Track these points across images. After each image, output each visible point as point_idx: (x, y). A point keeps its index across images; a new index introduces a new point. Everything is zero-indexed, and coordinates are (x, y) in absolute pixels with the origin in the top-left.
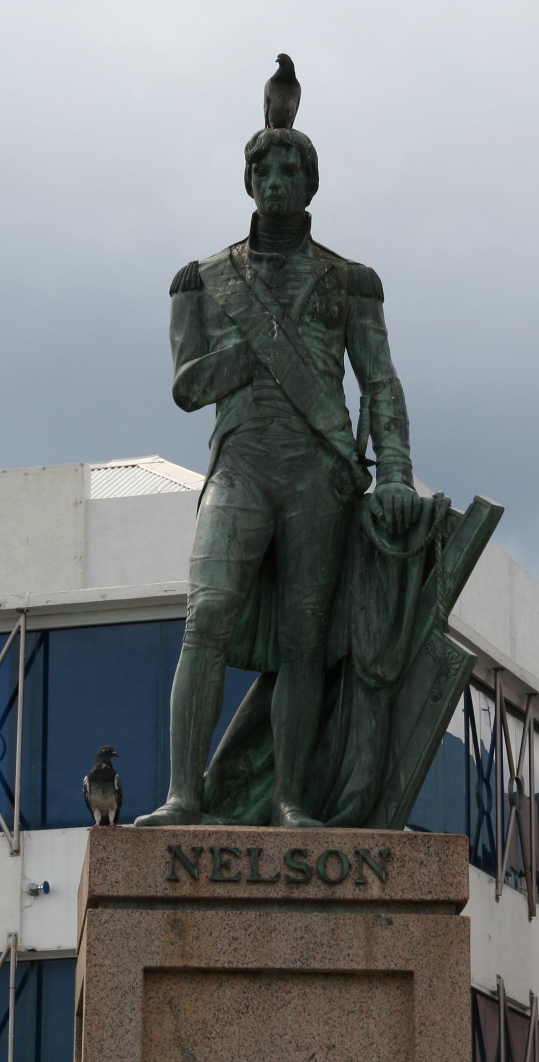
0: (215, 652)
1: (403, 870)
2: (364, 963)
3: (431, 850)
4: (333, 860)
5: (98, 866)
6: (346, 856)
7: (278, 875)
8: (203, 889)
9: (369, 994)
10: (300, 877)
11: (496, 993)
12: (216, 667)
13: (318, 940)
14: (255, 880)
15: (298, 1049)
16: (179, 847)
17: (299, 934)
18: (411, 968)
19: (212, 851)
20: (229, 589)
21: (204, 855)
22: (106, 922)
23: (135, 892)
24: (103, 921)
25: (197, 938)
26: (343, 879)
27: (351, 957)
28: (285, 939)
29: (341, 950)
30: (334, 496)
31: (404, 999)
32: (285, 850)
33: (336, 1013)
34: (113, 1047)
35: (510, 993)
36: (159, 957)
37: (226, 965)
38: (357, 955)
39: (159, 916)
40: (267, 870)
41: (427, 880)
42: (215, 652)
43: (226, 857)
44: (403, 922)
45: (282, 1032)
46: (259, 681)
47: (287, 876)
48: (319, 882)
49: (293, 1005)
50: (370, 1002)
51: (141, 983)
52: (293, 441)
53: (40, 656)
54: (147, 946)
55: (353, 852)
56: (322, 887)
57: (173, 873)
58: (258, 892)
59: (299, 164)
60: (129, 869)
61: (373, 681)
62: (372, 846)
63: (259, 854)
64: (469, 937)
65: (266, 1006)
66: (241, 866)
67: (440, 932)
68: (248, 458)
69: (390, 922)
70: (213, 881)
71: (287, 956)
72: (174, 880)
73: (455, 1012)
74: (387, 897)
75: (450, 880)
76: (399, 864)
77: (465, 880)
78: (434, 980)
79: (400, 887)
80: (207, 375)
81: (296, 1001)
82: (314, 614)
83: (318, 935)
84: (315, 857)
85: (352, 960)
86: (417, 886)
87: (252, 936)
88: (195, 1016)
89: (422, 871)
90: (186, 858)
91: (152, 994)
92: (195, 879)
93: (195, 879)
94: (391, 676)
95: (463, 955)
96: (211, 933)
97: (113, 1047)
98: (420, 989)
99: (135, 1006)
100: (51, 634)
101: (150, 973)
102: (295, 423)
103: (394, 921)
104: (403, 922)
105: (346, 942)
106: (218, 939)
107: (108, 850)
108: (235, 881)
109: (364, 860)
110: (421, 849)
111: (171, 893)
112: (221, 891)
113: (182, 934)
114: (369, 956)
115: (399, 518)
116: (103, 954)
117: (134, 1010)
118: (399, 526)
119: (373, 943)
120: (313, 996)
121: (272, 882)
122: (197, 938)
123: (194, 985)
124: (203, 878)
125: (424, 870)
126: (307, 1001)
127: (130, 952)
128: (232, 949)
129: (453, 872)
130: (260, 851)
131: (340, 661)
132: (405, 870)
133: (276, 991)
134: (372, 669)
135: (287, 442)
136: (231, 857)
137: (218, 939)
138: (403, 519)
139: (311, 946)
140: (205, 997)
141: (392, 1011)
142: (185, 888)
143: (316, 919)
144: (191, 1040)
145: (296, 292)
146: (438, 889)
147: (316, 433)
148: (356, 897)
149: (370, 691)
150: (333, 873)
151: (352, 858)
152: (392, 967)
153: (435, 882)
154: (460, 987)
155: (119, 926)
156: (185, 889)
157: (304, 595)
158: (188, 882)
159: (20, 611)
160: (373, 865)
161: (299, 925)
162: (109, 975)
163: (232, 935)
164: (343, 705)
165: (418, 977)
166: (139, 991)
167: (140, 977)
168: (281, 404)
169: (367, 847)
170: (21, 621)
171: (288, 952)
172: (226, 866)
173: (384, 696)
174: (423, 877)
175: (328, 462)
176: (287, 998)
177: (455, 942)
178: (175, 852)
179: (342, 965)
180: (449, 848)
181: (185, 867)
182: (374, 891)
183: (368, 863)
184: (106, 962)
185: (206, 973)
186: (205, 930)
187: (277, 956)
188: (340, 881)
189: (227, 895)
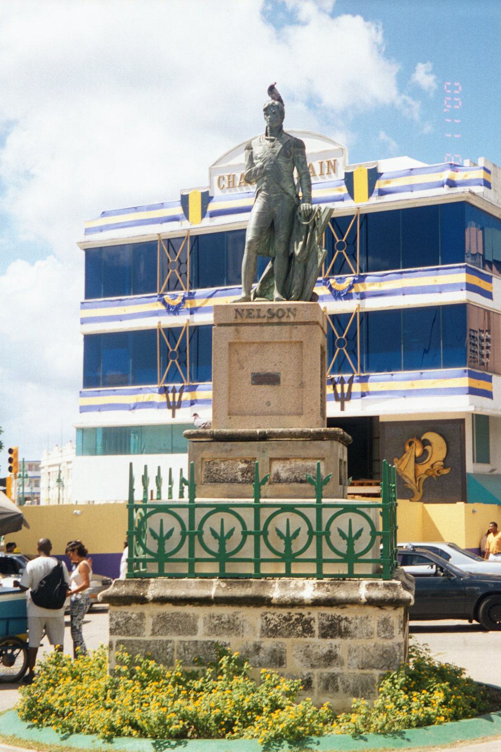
14: (259, 317)
18: (302, 340)
23: (225, 322)
39: (232, 328)
40: (262, 314)
43: (251, 311)
58: (259, 321)
72: (236, 317)
108: (254, 317)
112: (249, 321)
114: (291, 337)
137: (247, 333)
143: (276, 328)
156: (239, 321)
165: (304, 342)
172: (251, 313)
178: (237, 311)
182: (292, 319)
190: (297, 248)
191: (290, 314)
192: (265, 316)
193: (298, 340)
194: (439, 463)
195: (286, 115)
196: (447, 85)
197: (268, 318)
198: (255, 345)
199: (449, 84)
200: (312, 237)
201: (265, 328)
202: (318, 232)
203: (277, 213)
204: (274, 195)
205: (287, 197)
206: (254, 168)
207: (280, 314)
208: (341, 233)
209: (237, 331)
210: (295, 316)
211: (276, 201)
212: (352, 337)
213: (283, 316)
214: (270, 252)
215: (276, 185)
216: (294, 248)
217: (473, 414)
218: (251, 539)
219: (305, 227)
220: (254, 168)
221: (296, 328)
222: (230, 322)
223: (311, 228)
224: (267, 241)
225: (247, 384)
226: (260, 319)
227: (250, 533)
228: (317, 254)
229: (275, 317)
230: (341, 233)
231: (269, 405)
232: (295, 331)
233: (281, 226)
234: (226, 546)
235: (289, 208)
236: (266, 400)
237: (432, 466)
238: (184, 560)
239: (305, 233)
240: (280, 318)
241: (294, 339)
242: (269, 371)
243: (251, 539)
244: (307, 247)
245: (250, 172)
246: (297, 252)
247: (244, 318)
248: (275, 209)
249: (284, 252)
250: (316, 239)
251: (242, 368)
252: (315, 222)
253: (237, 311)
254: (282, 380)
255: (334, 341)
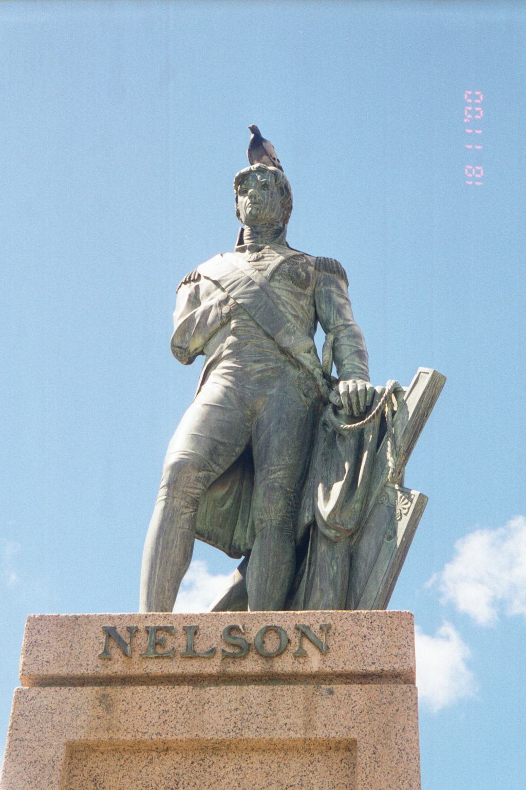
1: (344, 643)
2: (302, 732)
3: (375, 624)
4: (273, 636)
5: (31, 648)
6: (285, 632)
8: (136, 667)
9: (310, 768)
12: (183, 517)
13: (253, 711)
14: (191, 654)
16: (115, 628)
17: (234, 705)
18: (353, 735)
19: (147, 630)
21: (138, 635)
22: (33, 698)
23: (64, 671)
24: (30, 698)
26: (282, 653)
27: (288, 726)
31: (349, 772)
36: (84, 730)
39: (89, 692)
40: (202, 646)
41: (370, 652)
43: (161, 635)
44: (345, 692)
46: (187, 459)
47: (223, 651)
48: (256, 657)
49: (227, 781)
50: (311, 775)
52: (263, 357)
54: (72, 720)
55: (293, 628)
56: (260, 662)
57: (106, 652)
58: (192, 667)
60: (62, 650)
62: (312, 622)
63: (196, 633)
64: (416, 704)
65: (198, 782)
67: (384, 701)
69: (331, 692)
71: (218, 727)
72: (106, 656)
73: (402, 778)
74: (328, 670)
76: (341, 638)
77: (412, 652)
78: (379, 746)
79: (341, 660)
81: (230, 775)
82: (281, 487)
83: (254, 705)
85: (289, 729)
87: (184, 709)
89: (364, 644)
91: (76, 772)
95: (410, 722)
96: (140, 707)
98: (363, 756)
99: (53, 779)
103: (335, 691)
104: (345, 692)
107: (42, 633)
108: (169, 656)
110: (364, 624)
111: (104, 672)
112: (155, 667)
113: (109, 708)
114: (309, 725)
116: (26, 729)
117: (52, 783)
118: (355, 408)
119: (312, 712)
120: (249, 771)
122: (126, 712)
125: (367, 643)
126: (242, 776)
127: (54, 727)
128: (161, 721)
129: (398, 644)
131: (308, 528)
132: (347, 643)
133: (209, 767)
135: (259, 358)
136: (167, 636)
137: (145, 712)
139: (246, 717)
140: (134, 774)
141: (335, 784)
142: (116, 666)
143: (252, 691)
147: (284, 351)
148: (295, 669)
150: (271, 645)
153: (379, 653)
154: (407, 754)
155: (45, 702)
156: (118, 667)
157: (275, 472)
161: (234, 696)
162: (29, 749)
163: (162, 708)
164: (310, 564)
165: (361, 745)
169: (307, 624)
171: (222, 722)
174: (366, 649)
177: (401, 709)
178: (110, 633)
181: (119, 646)
182: (314, 663)
183: (307, 637)
184: (28, 736)
185: (136, 748)
186: (134, 704)
187: (209, 726)
189: (159, 672)
190: (327, 497)
191: (308, 646)
192: (213, 651)
193: (337, 733)
195: (293, 192)
196: (467, 94)
197: (226, 656)
198: (170, 760)
199: (470, 93)
200: (376, 462)
201: (211, 691)
202: (394, 443)
203: (264, 415)
204: (259, 367)
205: (294, 373)
206: (199, 310)
207: (271, 645)
209: (106, 703)
210: (324, 650)
211: (263, 383)
213: (280, 653)
214: (238, 533)
215: (266, 342)
216: (314, 496)
219: (352, 442)
220: (199, 310)
222: (79, 672)
223: (370, 438)
224: (228, 504)
226: (196, 663)
228: (392, 508)
229: (252, 654)
232: (325, 704)
233: (275, 443)
235: (300, 403)
239: (352, 458)
240: (268, 657)
241: (320, 733)
244: (359, 493)
245: (191, 319)
246: (325, 508)
247: (136, 657)
248: (260, 404)
249: (284, 522)
250: (390, 464)
252: (383, 419)
253: (110, 633)
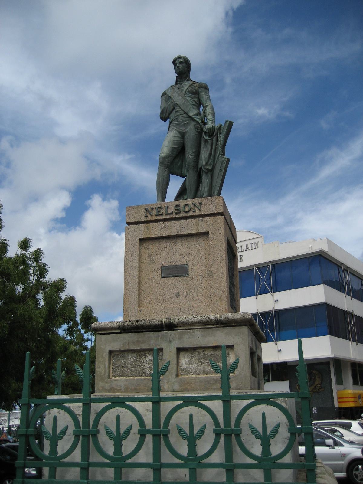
0: (165, 168)
7: (173, 212)
10: (178, 212)
11: (347, 310)
15: (180, 255)
17: (178, 226)
20: (168, 152)
25: (152, 230)
28: (175, 228)
29: (189, 229)
30: (196, 130)
32: (174, 206)
33: (190, 245)
34: (132, 259)
35: (349, 310)
37: (160, 236)
38: (194, 229)
42: (165, 168)
43: (159, 209)
45: (176, 251)
51: (138, 243)
53: (274, 269)
58: (168, 217)
59: (184, 62)
60: (135, 215)
61: (206, 170)
66: (163, 211)
68: (175, 126)
69: (202, 220)
70: (156, 215)
72: (146, 217)
75: (218, 207)
80: (165, 110)
84: (182, 206)
86: (209, 210)
88: (153, 250)
90: (149, 211)
92: (152, 216)
93: (152, 216)
94: (210, 168)
97: (132, 259)
100: (275, 265)
101: (142, 240)
102: (185, 115)
105: (191, 227)
106: (158, 230)
108: (162, 215)
109: (195, 205)
111: (146, 220)
112: (158, 218)
113: (148, 229)
115: (209, 131)
118: (210, 133)
121: (171, 214)
123: (153, 242)
124: (154, 215)
130: (168, 207)
134: (205, 167)
137: (158, 230)
138: (211, 131)
143: (183, 222)
144: (153, 256)
145: (184, 88)
146: (215, 210)
147: (190, 117)
149: (207, 173)
151: (192, 206)
152: (203, 231)
156: (149, 218)
158: (150, 216)
159: (270, 262)
160: (197, 206)
166: (138, 245)
167: (138, 241)
168: (181, 112)
169: (195, 202)
170: (270, 263)
173: (209, 174)
175: (193, 123)
176: (177, 243)
179: (190, 232)
180: (217, 200)
182: (198, 213)
184: (130, 238)
188: (189, 211)
194: (318, 385)
201: (173, 222)
208: (263, 274)
212: (271, 324)
217: (333, 359)
218: (149, 438)
221: (202, 220)
225: (157, 277)
227: (149, 432)
230: (263, 274)
231: (179, 296)
234: (123, 448)
236: (175, 291)
237: (315, 387)
238: (75, 465)
242: (178, 263)
243: (149, 438)
251: (152, 262)
254: (190, 270)
255: (263, 326)
